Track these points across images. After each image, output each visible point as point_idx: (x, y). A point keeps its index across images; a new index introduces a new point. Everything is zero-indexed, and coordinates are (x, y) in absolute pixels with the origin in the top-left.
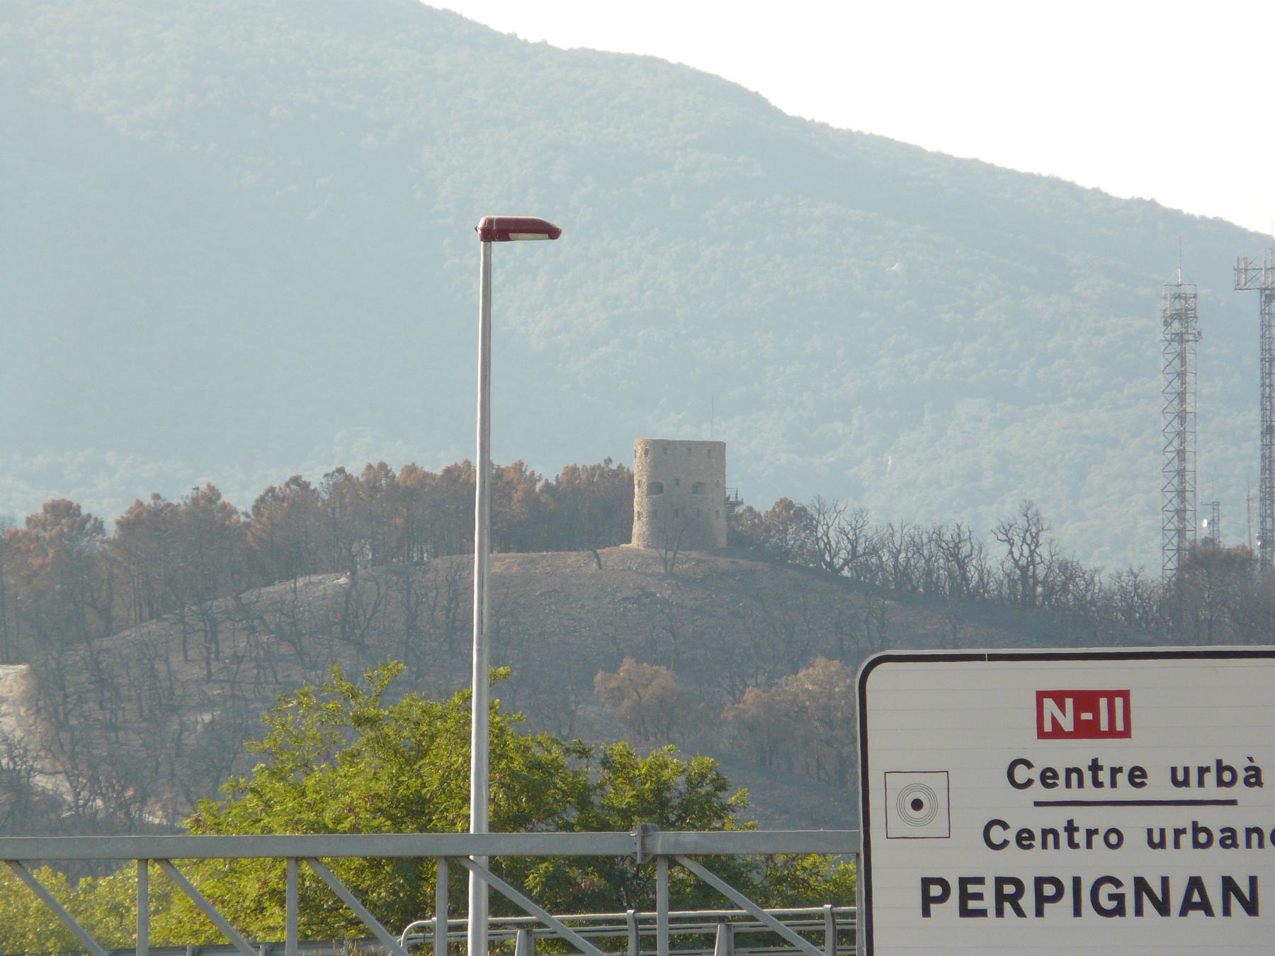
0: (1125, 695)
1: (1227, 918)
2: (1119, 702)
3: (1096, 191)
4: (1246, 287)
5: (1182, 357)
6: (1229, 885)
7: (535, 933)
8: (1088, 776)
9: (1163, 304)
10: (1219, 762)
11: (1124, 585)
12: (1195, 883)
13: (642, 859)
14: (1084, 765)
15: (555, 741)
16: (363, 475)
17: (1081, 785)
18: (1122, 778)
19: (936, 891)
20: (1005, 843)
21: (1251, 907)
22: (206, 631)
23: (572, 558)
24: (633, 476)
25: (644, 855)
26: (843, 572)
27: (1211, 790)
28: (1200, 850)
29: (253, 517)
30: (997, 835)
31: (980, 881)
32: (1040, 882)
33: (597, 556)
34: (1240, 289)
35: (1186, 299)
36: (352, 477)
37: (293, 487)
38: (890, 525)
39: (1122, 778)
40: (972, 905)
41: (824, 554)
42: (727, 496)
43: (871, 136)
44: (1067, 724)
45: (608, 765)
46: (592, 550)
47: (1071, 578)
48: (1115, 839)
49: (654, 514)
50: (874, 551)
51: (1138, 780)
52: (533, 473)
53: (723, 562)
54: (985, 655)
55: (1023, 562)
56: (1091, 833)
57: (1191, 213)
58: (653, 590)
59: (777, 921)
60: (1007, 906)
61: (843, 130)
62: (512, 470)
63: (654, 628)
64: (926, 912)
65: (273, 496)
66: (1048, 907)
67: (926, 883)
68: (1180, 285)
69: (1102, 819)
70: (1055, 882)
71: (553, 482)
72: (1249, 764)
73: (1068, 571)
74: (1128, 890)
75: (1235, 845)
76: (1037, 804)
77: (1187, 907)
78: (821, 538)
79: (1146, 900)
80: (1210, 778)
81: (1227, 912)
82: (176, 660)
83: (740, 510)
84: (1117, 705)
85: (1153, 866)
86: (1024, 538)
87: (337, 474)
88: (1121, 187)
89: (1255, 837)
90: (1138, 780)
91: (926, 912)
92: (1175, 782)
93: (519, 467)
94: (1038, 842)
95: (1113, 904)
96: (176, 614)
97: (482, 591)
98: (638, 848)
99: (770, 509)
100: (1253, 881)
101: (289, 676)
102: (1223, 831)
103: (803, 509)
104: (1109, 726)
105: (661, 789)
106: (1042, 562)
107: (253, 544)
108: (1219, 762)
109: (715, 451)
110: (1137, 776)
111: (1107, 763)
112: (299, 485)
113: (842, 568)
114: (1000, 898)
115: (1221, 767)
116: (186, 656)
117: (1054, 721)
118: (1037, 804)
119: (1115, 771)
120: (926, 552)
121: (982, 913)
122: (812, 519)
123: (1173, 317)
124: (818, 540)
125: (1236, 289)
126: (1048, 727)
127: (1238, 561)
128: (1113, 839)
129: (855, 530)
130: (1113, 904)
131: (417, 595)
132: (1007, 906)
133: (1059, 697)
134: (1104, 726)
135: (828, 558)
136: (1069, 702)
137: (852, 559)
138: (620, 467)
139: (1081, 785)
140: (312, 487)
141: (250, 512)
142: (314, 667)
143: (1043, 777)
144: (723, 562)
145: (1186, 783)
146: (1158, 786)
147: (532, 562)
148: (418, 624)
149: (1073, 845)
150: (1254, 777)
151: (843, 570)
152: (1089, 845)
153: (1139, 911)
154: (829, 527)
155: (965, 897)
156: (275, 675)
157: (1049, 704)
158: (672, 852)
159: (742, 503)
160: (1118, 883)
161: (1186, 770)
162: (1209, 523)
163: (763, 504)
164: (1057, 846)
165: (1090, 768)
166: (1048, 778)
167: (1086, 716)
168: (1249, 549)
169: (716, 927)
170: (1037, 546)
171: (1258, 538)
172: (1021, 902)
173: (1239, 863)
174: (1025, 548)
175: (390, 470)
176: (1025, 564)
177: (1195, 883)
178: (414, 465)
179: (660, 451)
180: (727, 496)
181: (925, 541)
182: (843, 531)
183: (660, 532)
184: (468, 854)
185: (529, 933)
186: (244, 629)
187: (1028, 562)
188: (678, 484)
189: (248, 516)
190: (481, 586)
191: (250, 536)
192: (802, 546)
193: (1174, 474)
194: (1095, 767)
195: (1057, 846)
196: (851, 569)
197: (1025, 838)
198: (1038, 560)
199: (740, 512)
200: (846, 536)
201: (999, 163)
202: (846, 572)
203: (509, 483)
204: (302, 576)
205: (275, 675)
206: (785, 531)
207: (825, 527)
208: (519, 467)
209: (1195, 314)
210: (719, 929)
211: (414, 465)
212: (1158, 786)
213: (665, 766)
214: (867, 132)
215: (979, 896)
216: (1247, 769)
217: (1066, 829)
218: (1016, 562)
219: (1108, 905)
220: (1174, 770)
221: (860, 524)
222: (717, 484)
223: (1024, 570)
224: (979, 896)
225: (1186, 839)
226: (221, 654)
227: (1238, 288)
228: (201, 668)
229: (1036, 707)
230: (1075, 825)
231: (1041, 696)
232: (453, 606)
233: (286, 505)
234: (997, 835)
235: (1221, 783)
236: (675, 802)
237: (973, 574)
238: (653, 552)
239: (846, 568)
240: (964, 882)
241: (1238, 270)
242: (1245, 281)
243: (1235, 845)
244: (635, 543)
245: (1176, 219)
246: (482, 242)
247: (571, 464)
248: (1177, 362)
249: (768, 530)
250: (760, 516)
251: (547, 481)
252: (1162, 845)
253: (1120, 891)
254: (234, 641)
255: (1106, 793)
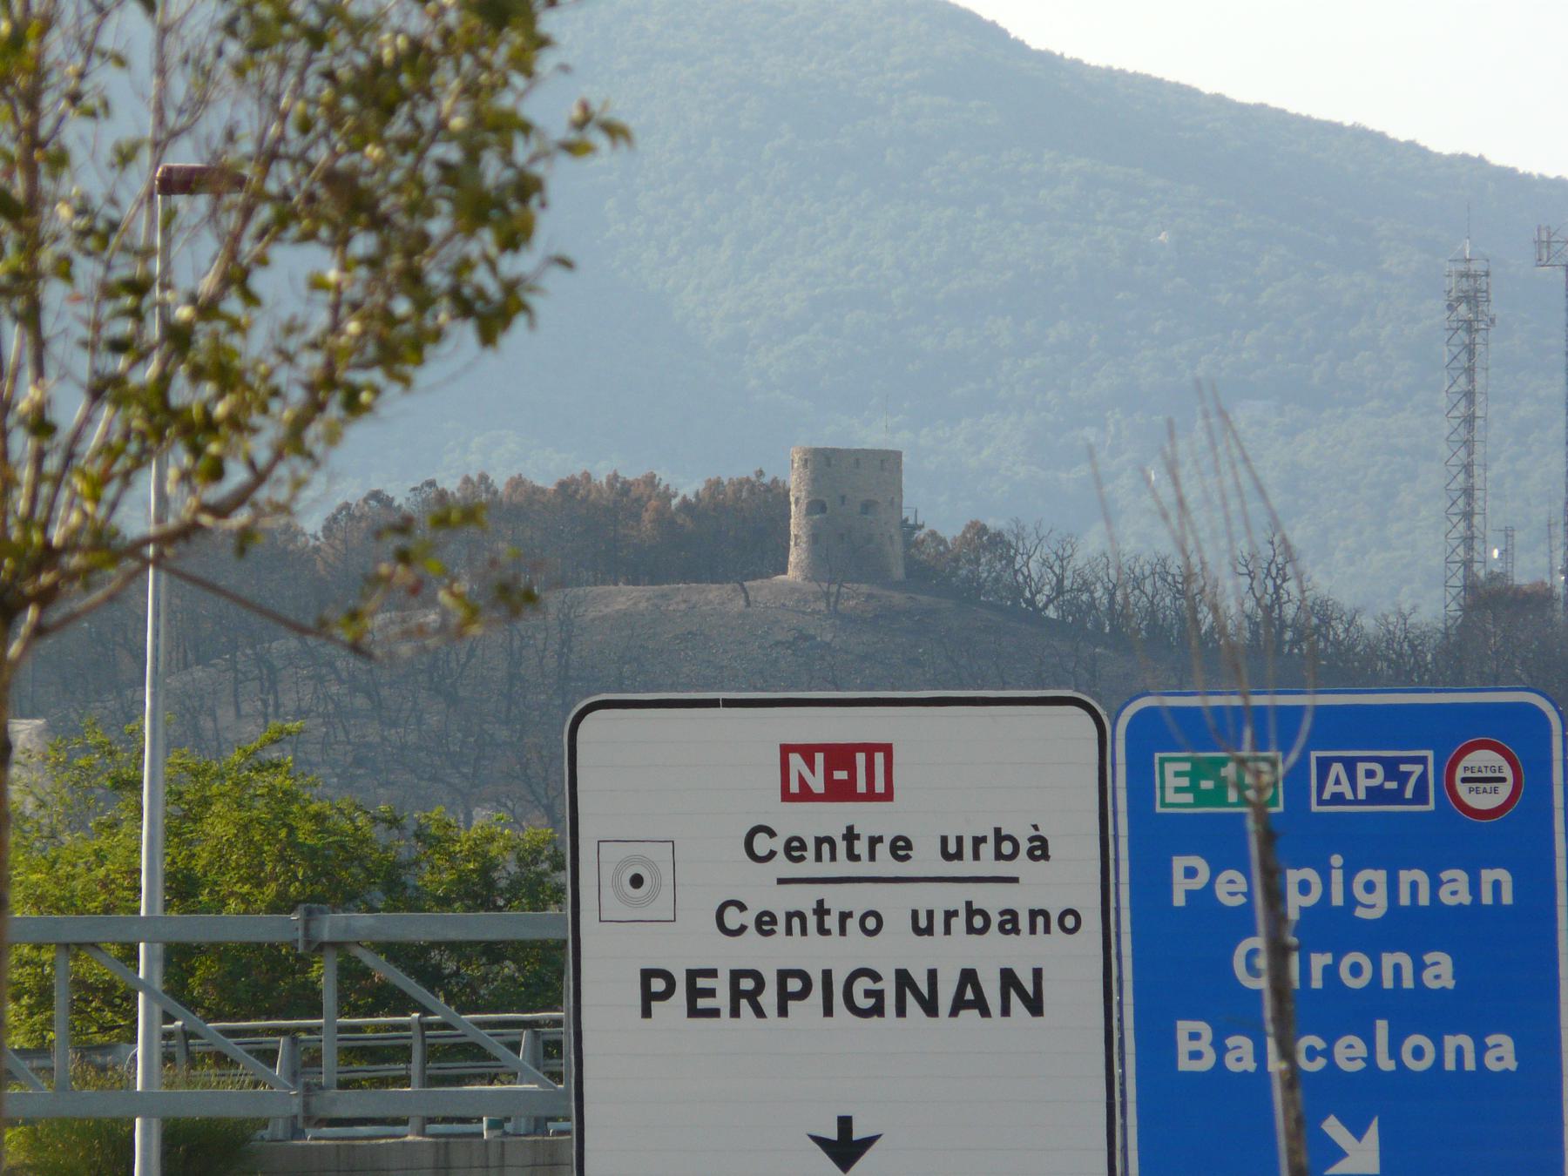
0: (887, 749)
1: (901, 1019)
2: (879, 758)
3: (1411, 145)
4: (1549, 263)
5: (1470, 350)
6: (1009, 979)
7: (302, 1041)
8: (841, 847)
9: (1451, 283)
10: (997, 831)
11: (1391, 628)
12: (969, 977)
13: (305, 948)
14: (838, 834)
15: (358, 808)
16: (458, 490)
17: (833, 858)
18: (883, 850)
19: (658, 985)
20: (743, 929)
21: (1035, 1006)
22: (261, 679)
23: (714, 593)
24: (789, 491)
25: (308, 943)
26: (1047, 612)
27: (988, 865)
28: (974, 937)
29: (322, 539)
30: (733, 918)
31: (712, 973)
32: (783, 975)
33: (744, 590)
34: (1543, 266)
35: (1475, 276)
36: (446, 493)
37: (373, 503)
38: (1104, 554)
39: (883, 850)
40: (703, 1003)
41: (1025, 589)
42: (903, 518)
43: (1135, 75)
44: (817, 784)
45: (422, 837)
46: (738, 583)
47: (1326, 621)
48: (873, 923)
49: (814, 538)
50: (1086, 586)
51: (796, 854)
52: (667, 487)
53: (899, 598)
54: (719, 700)
55: (1267, 600)
56: (844, 917)
57: (1527, 172)
58: (812, 632)
59: (478, 1030)
60: (744, 1004)
61: (1101, 68)
62: (641, 483)
63: (812, 678)
64: (647, 1013)
65: (348, 514)
66: (656, 1006)
67: (647, 975)
68: (1470, 260)
69: (856, 899)
70: (667, 976)
71: (691, 497)
72: (1034, 833)
73: (1323, 614)
74: (889, 986)
75: (1016, 930)
76: (781, 881)
77: (959, 1005)
78: (1020, 569)
79: (910, 999)
80: (987, 850)
81: (1006, 1011)
82: (226, 715)
83: (920, 534)
84: (1405, 770)
85: (919, 957)
86: (1269, 570)
87: (427, 489)
88: (1443, 140)
89: (1040, 920)
90: (796, 854)
91: (647, 1013)
92: (947, 856)
93: (650, 481)
94: (781, 927)
95: (870, 1002)
96: (226, 660)
97: (158, 621)
98: (300, 933)
99: (958, 533)
100: (1038, 973)
101: (364, 737)
102: (1002, 913)
103: (999, 534)
104: (800, 787)
105: (488, 867)
106: (1289, 601)
107: (323, 573)
108: (997, 831)
109: (888, 462)
110: (901, 848)
111: (865, 830)
112: (379, 501)
113: (1046, 606)
114: (736, 995)
115: (1000, 837)
116: (238, 709)
117: (802, 781)
118: (781, 881)
119: (874, 841)
120: (1149, 589)
121: (714, 1013)
122: (1009, 545)
123: (1459, 300)
124: (1016, 572)
125: (1537, 266)
126: (794, 787)
127: (1537, 600)
128: (871, 923)
129: (1062, 561)
130: (870, 1002)
131: (522, 638)
132: (744, 1003)
133: (807, 752)
134: (861, 787)
135: (1028, 594)
136: (819, 758)
137: (1057, 597)
138: (775, 481)
139: (833, 858)
140: (396, 503)
141: (320, 534)
142: (394, 724)
143: (788, 849)
144: (899, 598)
145: (958, 855)
146: (926, 859)
147: (664, 596)
148: (523, 672)
149: (823, 931)
150: (1040, 849)
151: (1047, 608)
152: (843, 931)
153: (901, 1011)
154: (1029, 557)
155: (694, 993)
156: (347, 733)
157: (796, 760)
158: (341, 938)
159: (922, 527)
160: (876, 977)
161: (960, 840)
162: (1500, 554)
163: (951, 531)
164: (804, 932)
165: (845, 837)
166: (794, 849)
167: (841, 775)
168: (1549, 585)
169: (521, 1034)
170: (1284, 580)
171: (1562, 572)
172: (760, 999)
173: (1021, 953)
174: (1270, 583)
175: (492, 485)
176: (1269, 603)
177: (969, 977)
178: (520, 475)
179: (823, 462)
180: (903, 518)
181: (1147, 573)
182: (1045, 562)
183: (823, 561)
184: (132, 939)
185: (295, 1042)
186: (311, 678)
187: (1272, 601)
188: (843, 503)
189: (317, 539)
190: (156, 615)
191: (320, 566)
192: (997, 580)
193: (1459, 493)
194: (851, 836)
195: (804, 932)
196: (1057, 608)
197: (765, 923)
198: (1285, 598)
199: (922, 536)
200: (1051, 568)
201: (1292, 109)
202: (1051, 613)
203: (637, 500)
204: (383, 612)
205: (347, 733)
206: (977, 561)
207: (1025, 557)
208: (650, 481)
209: (1487, 297)
210: (525, 1037)
211: (520, 475)
212: (926, 859)
213: (491, 839)
214: (1130, 70)
215: (711, 993)
216: (1031, 839)
217: (815, 912)
218: (1258, 601)
219: (864, 1003)
220: (944, 840)
221: (1069, 552)
222: (892, 503)
223: (1268, 610)
224: (711, 993)
225: (959, 924)
226: (282, 709)
227: (1539, 262)
228: (257, 726)
229: (894, 766)
230: (826, 906)
231: (786, 750)
232: (565, 650)
233: (363, 525)
234: (733, 918)
235: (999, 856)
236: (503, 884)
237: (1206, 618)
238: (814, 586)
239: (1051, 607)
240: (692, 975)
241: (1539, 243)
242: (1548, 256)
243: (1016, 930)
244: (793, 574)
245: (1509, 179)
246: (159, 197)
247: (713, 477)
248: (1464, 357)
249: (956, 559)
250: (946, 542)
251: (684, 497)
252: (929, 931)
253: (878, 986)
254: (298, 693)
255: (863, 868)
